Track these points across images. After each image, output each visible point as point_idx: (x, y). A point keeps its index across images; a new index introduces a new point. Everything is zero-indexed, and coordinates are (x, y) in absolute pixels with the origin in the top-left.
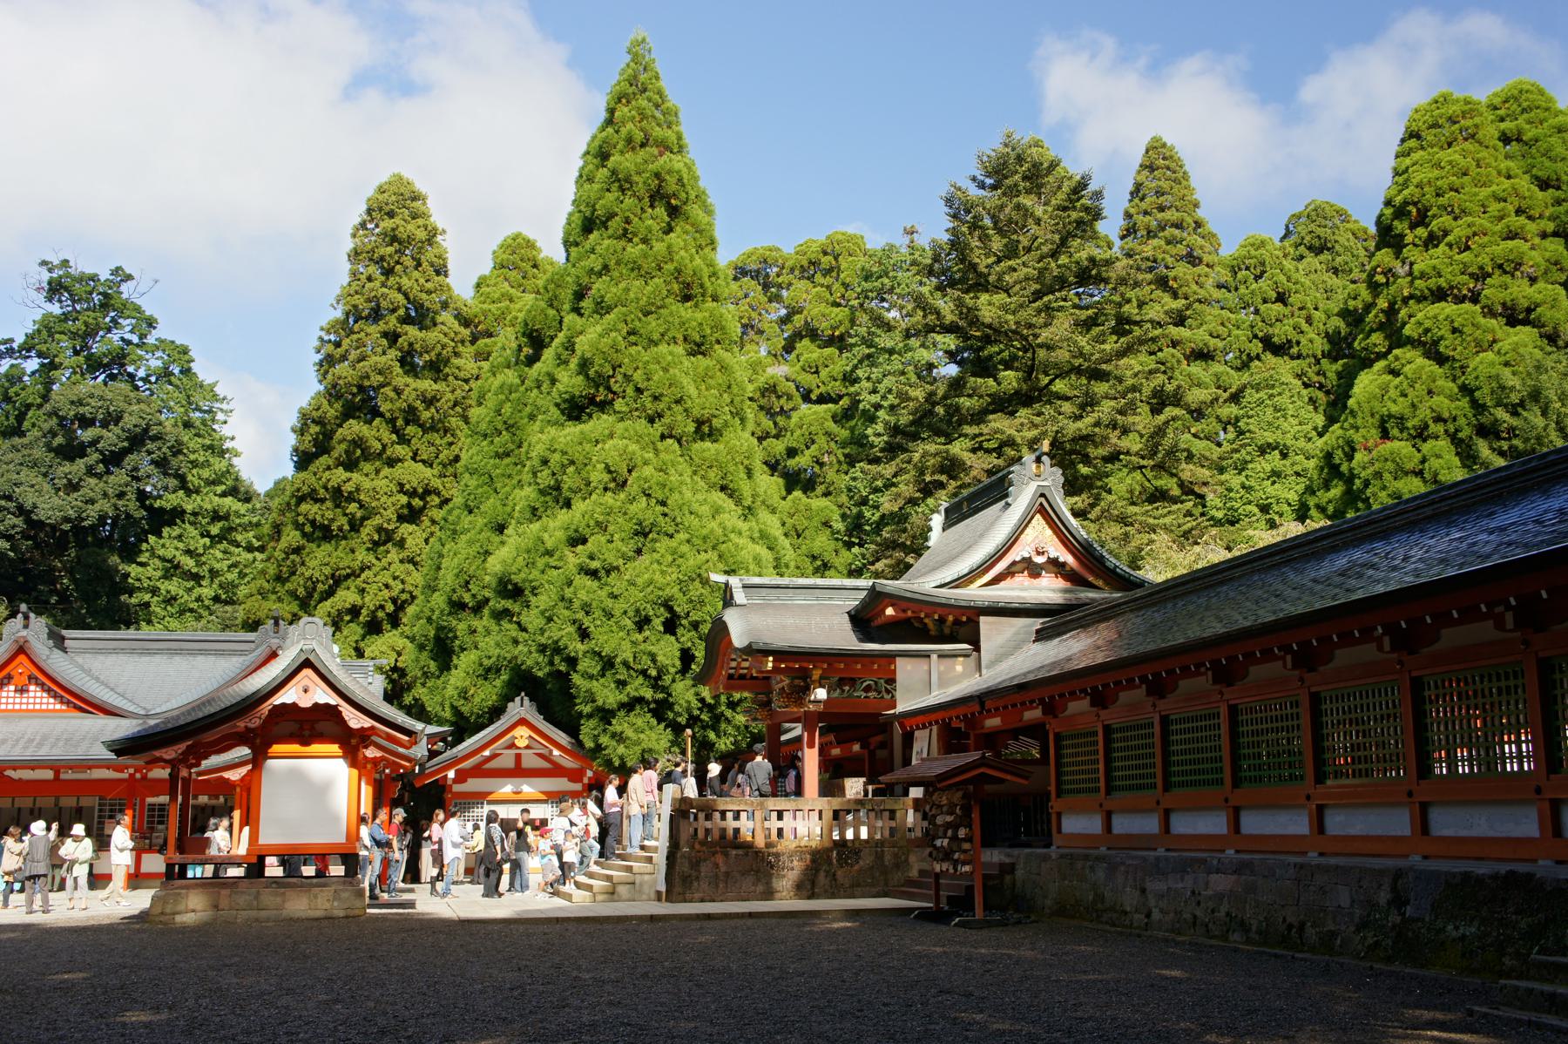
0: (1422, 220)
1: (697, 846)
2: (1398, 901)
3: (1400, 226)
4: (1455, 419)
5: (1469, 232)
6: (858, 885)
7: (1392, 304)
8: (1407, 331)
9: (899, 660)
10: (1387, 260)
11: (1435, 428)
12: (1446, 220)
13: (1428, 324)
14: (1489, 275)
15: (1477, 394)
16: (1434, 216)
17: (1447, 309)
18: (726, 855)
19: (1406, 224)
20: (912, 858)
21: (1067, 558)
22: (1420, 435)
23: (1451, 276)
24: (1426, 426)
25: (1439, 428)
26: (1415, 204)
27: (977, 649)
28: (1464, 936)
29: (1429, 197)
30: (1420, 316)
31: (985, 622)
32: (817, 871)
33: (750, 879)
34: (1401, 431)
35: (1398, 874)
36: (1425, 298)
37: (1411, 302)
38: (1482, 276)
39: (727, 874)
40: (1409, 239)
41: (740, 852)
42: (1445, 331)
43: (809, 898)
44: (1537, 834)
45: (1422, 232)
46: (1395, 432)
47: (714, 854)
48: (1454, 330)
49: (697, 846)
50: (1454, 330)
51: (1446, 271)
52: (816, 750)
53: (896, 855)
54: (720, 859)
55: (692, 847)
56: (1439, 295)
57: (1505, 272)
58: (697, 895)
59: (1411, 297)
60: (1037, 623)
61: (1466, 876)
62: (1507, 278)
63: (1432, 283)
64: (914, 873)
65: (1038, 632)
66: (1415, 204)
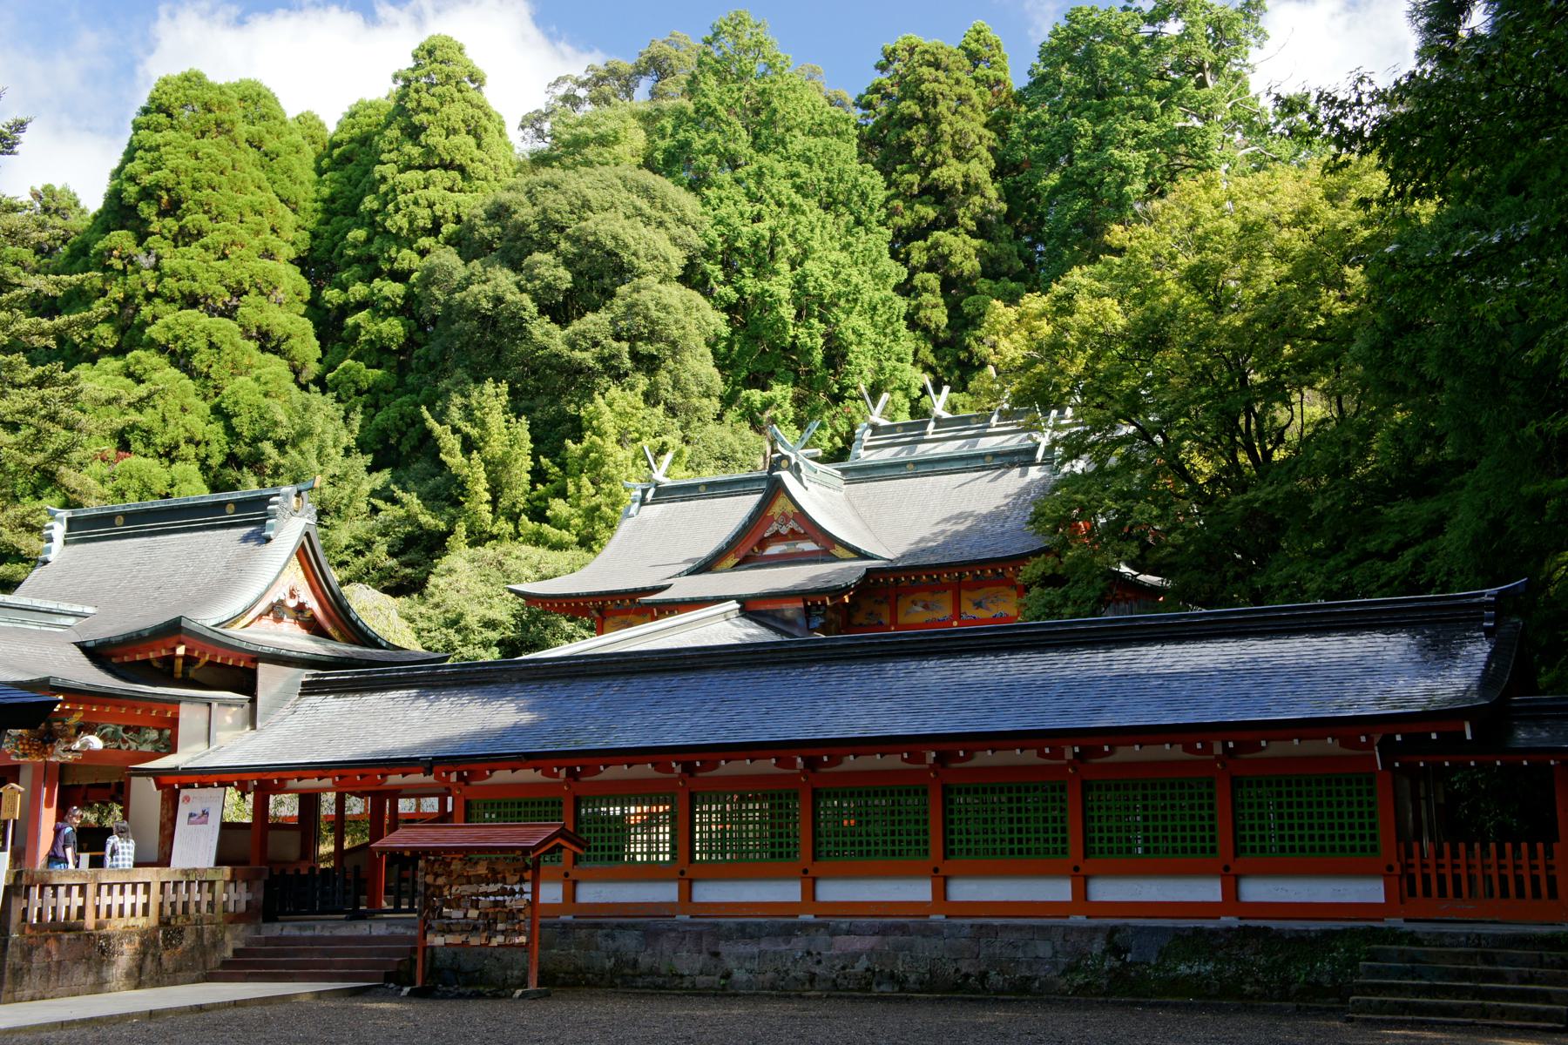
0: (173, 208)
1: (27, 931)
2: (1116, 950)
3: (147, 210)
4: (207, 444)
5: (229, 239)
6: (180, 970)
7: (129, 298)
8: (153, 331)
9: (183, 706)
10: (127, 244)
11: (187, 450)
12: (201, 219)
13: (180, 331)
14: (246, 293)
15: (235, 421)
16: (188, 210)
17: (197, 318)
18: (58, 939)
19: (154, 210)
20: (228, 936)
21: (313, 605)
22: (167, 455)
23: (208, 285)
24: (177, 447)
25: (189, 451)
26: (168, 190)
27: (253, 701)
28: (1199, 973)
29: (185, 189)
30: (169, 319)
31: (264, 670)
32: (145, 954)
33: (82, 968)
34: (147, 446)
35: (1114, 930)
36: (173, 300)
37: (157, 301)
38: (239, 292)
39: (59, 963)
40: (155, 226)
41: (72, 935)
42: (201, 344)
43: (136, 988)
44: (1382, 900)
45: (170, 222)
46: (137, 446)
47: (46, 939)
48: (211, 345)
49: (27, 931)
50: (211, 345)
51: (201, 275)
52: (53, 810)
53: (213, 933)
54: (52, 945)
55: (22, 932)
56: (191, 301)
57: (262, 293)
58: (28, 993)
59: (157, 294)
60: (305, 675)
61: (1198, 931)
62: (262, 299)
63: (186, 285)
64: (229, 954)
65: (304, 684)
66: (168, 190)
